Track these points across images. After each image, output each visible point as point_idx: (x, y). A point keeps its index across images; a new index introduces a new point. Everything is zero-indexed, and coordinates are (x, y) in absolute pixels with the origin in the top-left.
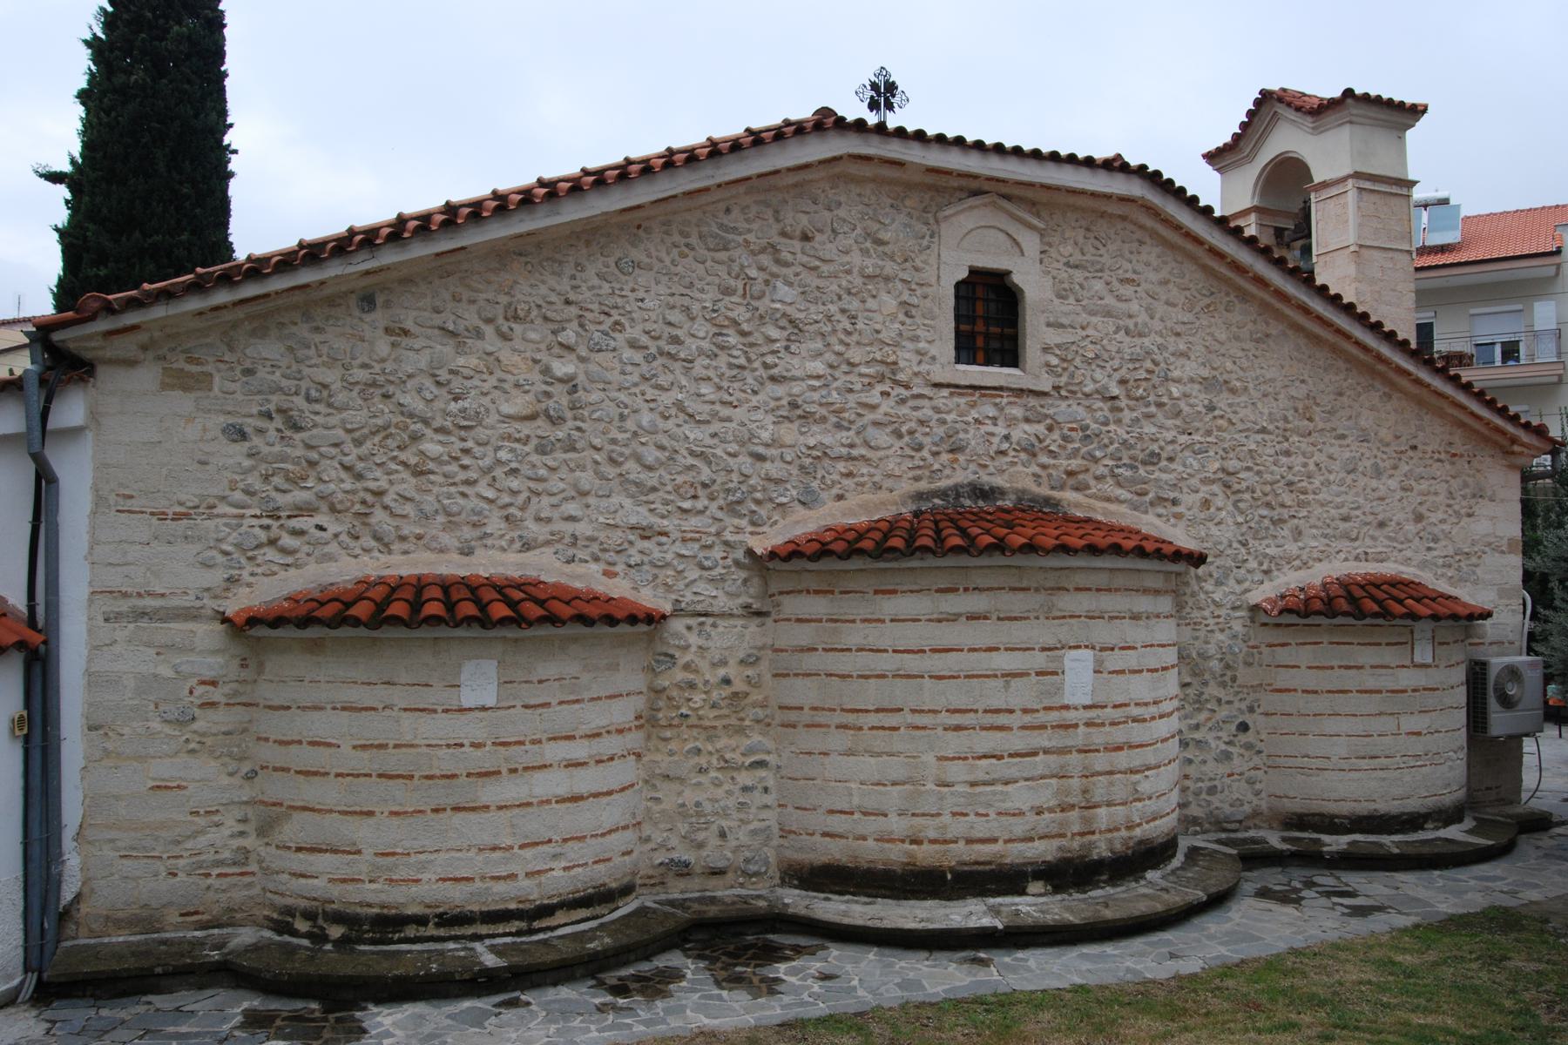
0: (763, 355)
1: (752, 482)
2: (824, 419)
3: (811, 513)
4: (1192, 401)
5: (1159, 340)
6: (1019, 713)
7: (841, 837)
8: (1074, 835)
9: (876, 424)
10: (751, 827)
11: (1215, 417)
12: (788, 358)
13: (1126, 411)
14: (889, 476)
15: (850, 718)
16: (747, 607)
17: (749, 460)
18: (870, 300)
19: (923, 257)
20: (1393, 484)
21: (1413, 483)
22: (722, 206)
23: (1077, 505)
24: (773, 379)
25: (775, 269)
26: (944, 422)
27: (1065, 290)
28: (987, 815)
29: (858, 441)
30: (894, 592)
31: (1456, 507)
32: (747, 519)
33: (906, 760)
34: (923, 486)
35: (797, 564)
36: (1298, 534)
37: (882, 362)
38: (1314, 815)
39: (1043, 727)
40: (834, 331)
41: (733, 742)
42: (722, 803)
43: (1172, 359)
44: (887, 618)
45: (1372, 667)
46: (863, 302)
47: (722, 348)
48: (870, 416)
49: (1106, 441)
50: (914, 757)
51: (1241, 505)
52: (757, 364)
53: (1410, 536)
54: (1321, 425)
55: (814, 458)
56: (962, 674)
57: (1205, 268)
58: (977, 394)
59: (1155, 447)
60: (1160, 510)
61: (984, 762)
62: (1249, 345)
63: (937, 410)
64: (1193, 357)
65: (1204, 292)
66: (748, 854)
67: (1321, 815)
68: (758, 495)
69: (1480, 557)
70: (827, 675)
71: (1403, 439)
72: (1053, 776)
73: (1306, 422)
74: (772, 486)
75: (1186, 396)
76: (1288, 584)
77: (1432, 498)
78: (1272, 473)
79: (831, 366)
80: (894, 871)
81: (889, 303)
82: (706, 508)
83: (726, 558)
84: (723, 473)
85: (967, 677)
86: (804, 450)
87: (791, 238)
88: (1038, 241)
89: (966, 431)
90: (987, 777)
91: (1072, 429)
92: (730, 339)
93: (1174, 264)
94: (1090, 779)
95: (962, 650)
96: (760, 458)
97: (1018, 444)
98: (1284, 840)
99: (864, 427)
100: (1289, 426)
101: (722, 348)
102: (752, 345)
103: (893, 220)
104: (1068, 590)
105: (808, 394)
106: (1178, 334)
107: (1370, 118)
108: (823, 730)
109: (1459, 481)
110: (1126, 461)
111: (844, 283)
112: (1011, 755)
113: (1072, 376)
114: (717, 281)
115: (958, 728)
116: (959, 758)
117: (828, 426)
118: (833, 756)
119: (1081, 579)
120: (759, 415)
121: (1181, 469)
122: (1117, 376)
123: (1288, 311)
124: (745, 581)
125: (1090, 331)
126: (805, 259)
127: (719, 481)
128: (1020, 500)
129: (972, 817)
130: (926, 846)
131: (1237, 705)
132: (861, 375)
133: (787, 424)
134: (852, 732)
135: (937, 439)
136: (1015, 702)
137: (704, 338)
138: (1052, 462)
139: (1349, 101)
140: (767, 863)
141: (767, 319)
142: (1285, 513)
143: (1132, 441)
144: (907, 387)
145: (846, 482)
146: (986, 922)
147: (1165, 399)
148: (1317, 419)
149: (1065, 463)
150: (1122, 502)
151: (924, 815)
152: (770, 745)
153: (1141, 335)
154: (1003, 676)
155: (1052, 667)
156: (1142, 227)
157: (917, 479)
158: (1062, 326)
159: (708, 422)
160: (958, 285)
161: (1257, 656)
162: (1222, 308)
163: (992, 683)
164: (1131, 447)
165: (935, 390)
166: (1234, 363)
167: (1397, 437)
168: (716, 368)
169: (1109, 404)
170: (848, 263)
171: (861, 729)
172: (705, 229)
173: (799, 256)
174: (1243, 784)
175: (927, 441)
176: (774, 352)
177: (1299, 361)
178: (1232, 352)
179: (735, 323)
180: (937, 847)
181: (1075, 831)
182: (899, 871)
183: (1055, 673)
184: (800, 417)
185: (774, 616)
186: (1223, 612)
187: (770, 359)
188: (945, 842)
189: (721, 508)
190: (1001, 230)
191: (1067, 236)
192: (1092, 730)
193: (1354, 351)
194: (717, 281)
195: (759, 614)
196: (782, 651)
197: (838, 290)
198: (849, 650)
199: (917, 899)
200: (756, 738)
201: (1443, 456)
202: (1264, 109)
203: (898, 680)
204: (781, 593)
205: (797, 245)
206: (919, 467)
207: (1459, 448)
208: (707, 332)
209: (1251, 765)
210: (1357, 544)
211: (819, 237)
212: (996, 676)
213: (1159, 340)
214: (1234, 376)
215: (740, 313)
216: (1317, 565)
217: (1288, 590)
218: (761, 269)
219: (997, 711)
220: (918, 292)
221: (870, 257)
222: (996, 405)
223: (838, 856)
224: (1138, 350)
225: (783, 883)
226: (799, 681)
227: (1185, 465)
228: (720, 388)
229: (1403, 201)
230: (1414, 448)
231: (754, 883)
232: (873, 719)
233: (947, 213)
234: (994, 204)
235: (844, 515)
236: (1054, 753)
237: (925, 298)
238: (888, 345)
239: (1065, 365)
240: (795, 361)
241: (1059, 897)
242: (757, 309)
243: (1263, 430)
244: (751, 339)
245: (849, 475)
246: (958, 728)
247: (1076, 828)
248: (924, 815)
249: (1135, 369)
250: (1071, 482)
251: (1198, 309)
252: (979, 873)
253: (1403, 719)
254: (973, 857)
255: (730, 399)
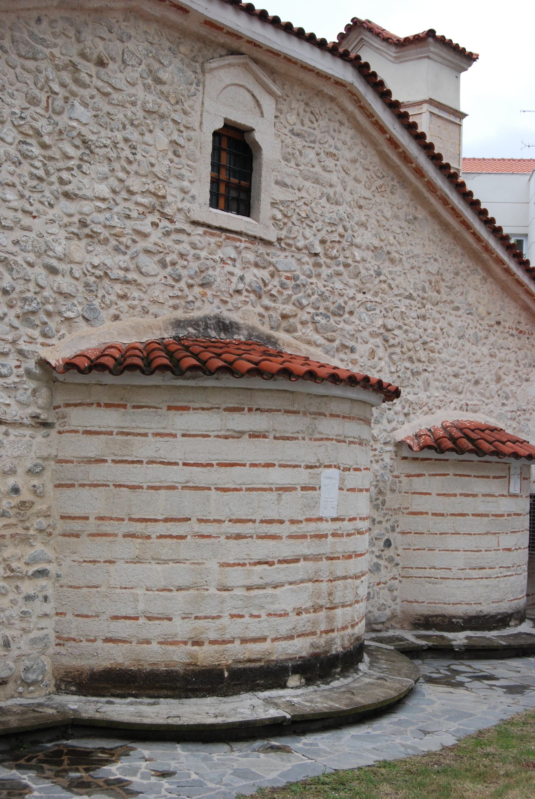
0: (59, 170)
1: (46, 293)
2: (106, 241)
3: (94, 330)
4: (368, 265)
5: (349, 210)
6: (287, 523)
7: (124, 641)
8: (322, 632)
9: (147, 252)
10: (32, 636)
11: (380, 281)
12: (80, 176)
13: (324, 267)
14: (154, 302)
15: (139, 527)
16: (36, 417)
17: (44, 272)
18: (147, 134)
19: (191, 103)
20: (485, 350)
21: (497, 352)
22: (35, 14)
23: (289, 345)
24: (67, 195)
25: (74, 88)
26: (198, 258)
27: (289, 154)
28: (259, 616)
29: (132, 267)
30: (187, 408)
31: (520, 373)
32: (39, 329)
33: (193, 566)
34: (180, 314)
35: (95, 377)
36: (427, 384)
37: (155, 194)
38: (437, 616)
39: (304, 537)
40: (119, 158)
41: (18, 551)
42: (7, 613)
43: (356, 228)
44: (179, 433)
45: (483, 495)
46: (142, 134)
47: (26, 157)
48: (142, 244)
49: (310, 292)
50: (198, 564)
51: (394, 357)
52: (54, 178)
53: (493, 394)
54: (445, 298)
55: (97, 277)
56: (244, 487)
57: (381, 154)
58: (223, 235)
59: (341, 301)
60: (342, 356)
61: (259, 568)
62: (404, 224)
63: (194, 246)
64: (369, 229)
65: (379, 174)
66: (28, 663)
67: (444, 616)
68: (50, 307)
69: (531, 414)
70: (116, 486)
71: (493, 315)
72: (310, 580)
73: (436, 294)
74: (61, 300)
75: (364, 260)
76: (420, 425)
77: (506, 364)
78: (414, 333)
79: (114, 192)
80: (176, 671)
81: (163, 142)
82: (5, 315)
83: (18, 367)
84: (22, 282)
85: (248, 489)
86: (90, 268)
87: (88, 60)
88: (274, 106)
89: (214, 268)
90: (261, 582)
91: (287, 278)
92: (33, 149)
93: (361, 147)
94: (334, 583)
95: (244, 465)
96: (53, 271)
97: (250, 285)
98: (418, 637)
99: (137, 253)
100: (426, 295)
101: (26, 157)
102: (51, 158)
103: (171, 63)
104: (325, 416)
105: (95, 215)
106: (360, 207)
107: (441, 57)
108: (110, 539)
109: (523, 352)
110: (321, 310)
111: (129, 114)
112: (280, 562)
113: (290, 231)
114: (25, 89)
115: (239, 537)
116: (239, 564)
117: (109, 248)
118: (120, 565)
119: (334, 407)
120: (54, 229)
121: (357, 322)
122: (320, 236)
123: (433, 200)
124: (34, 391)
125: (303, 194)
126: (100, 84)
127: (18, 289)
128: (250, 335)
129: (247, 619)
130: (207, 647)
131: (384, 524)
132: (137, 204)
133: (75, 242)
134: (139, 541)
135: (192, 272)
136: (286, 514)
137: (11, 144)
138: (273, 305)
139: (431, 40)
140: (43, 672)
141: (65, 136)
142: (420, 367)
143: (327, 294)
144: (172, 221)
145: (122, 304)
146: (273, 713)
147: (350, 261)
148: (443, 292)
149: (282, 307)
150: (318, 346)
151: (206, 618)
152: (51, 554)
153: (337, 203)
154: (278, 489)
155: (312, 483)
156: (344, 110)
157: (175, 307)
158: (285, 185)
159: (11, 229)
160: (216, 134)
161: (398, 484)
162: (388, 190)
163: (267, 495)
164: (326, 299)
165: (193, 227)
166: (395, 238)
167: (489, 313)
168: (20, 176)
169: (313, 259)
170: (134, 95)
171: (149, 537)
172: (17, 34)
173: (94, 79)
174: (386, 591)
175: (184, 273)
176: (69, 169)
177: (434, 242)
178: (394, 228)
179: (38, 134)
180: (216, 647)
181: (323, 629)
182: (182, 671)
183: (314, 489)
184: (88, 236)
185: (58, 428)
186: (378, 446)
187: (65, 175)
188: (224, 642)
189: (18, 317)
190: (249, 91)
191: (293, 106)
192: (336, 539)
193: (471, 240)
194: (25, 89)
195: (45, 425)
196: (67, 462)
197: (124, 119)
198: (140, 462)
199: (197, 697)
200: (39, 547)
201: (514, 332)
202: (353, 35)
203: (187, 491)
204: (67, 405)
205: (93, 69)
206: (178, 297)
207: (523, 327)
208: (14, 138)
209: (392, 575)
210: (462, 396)
211: (112, 66)
212: (271, 490)
213: (349, 210)
214: (394, 248)
215: (42, 124)
216: (438, 411)
217: (420, 430)
218: (63, 85)
219: (271, 522)
220: (185, 134)
221: (151, 93)
222: (236, 248)
223: (120, 660)
224: (334, 215)
225: (58, 690)
226: (85, 492)
227: (360, 320)
228: (22, 196)
229: (455, 127)
230: (498, 323)
231: (32, 692)
232: (161, 528)
233: (214, 65)
234: (245, 66)
235: (120, 334)
236: (310, 560)
237: (189, 140)
238: (160, 179)
239: (285, 220)
240: (86, 181)
241: (311, 688)
242: (57, 124)
243: (410, 297)
244: (49, 153)
245: (124, 297)
246: (239, 537)
247: (323, 627)
248: (206, 618)
249: (332, 232)
250: (284, 324)
251: (373, 188)
252: (251, 669)
253: (502, 537)
254: (247, 656)
255: (30, 209)
